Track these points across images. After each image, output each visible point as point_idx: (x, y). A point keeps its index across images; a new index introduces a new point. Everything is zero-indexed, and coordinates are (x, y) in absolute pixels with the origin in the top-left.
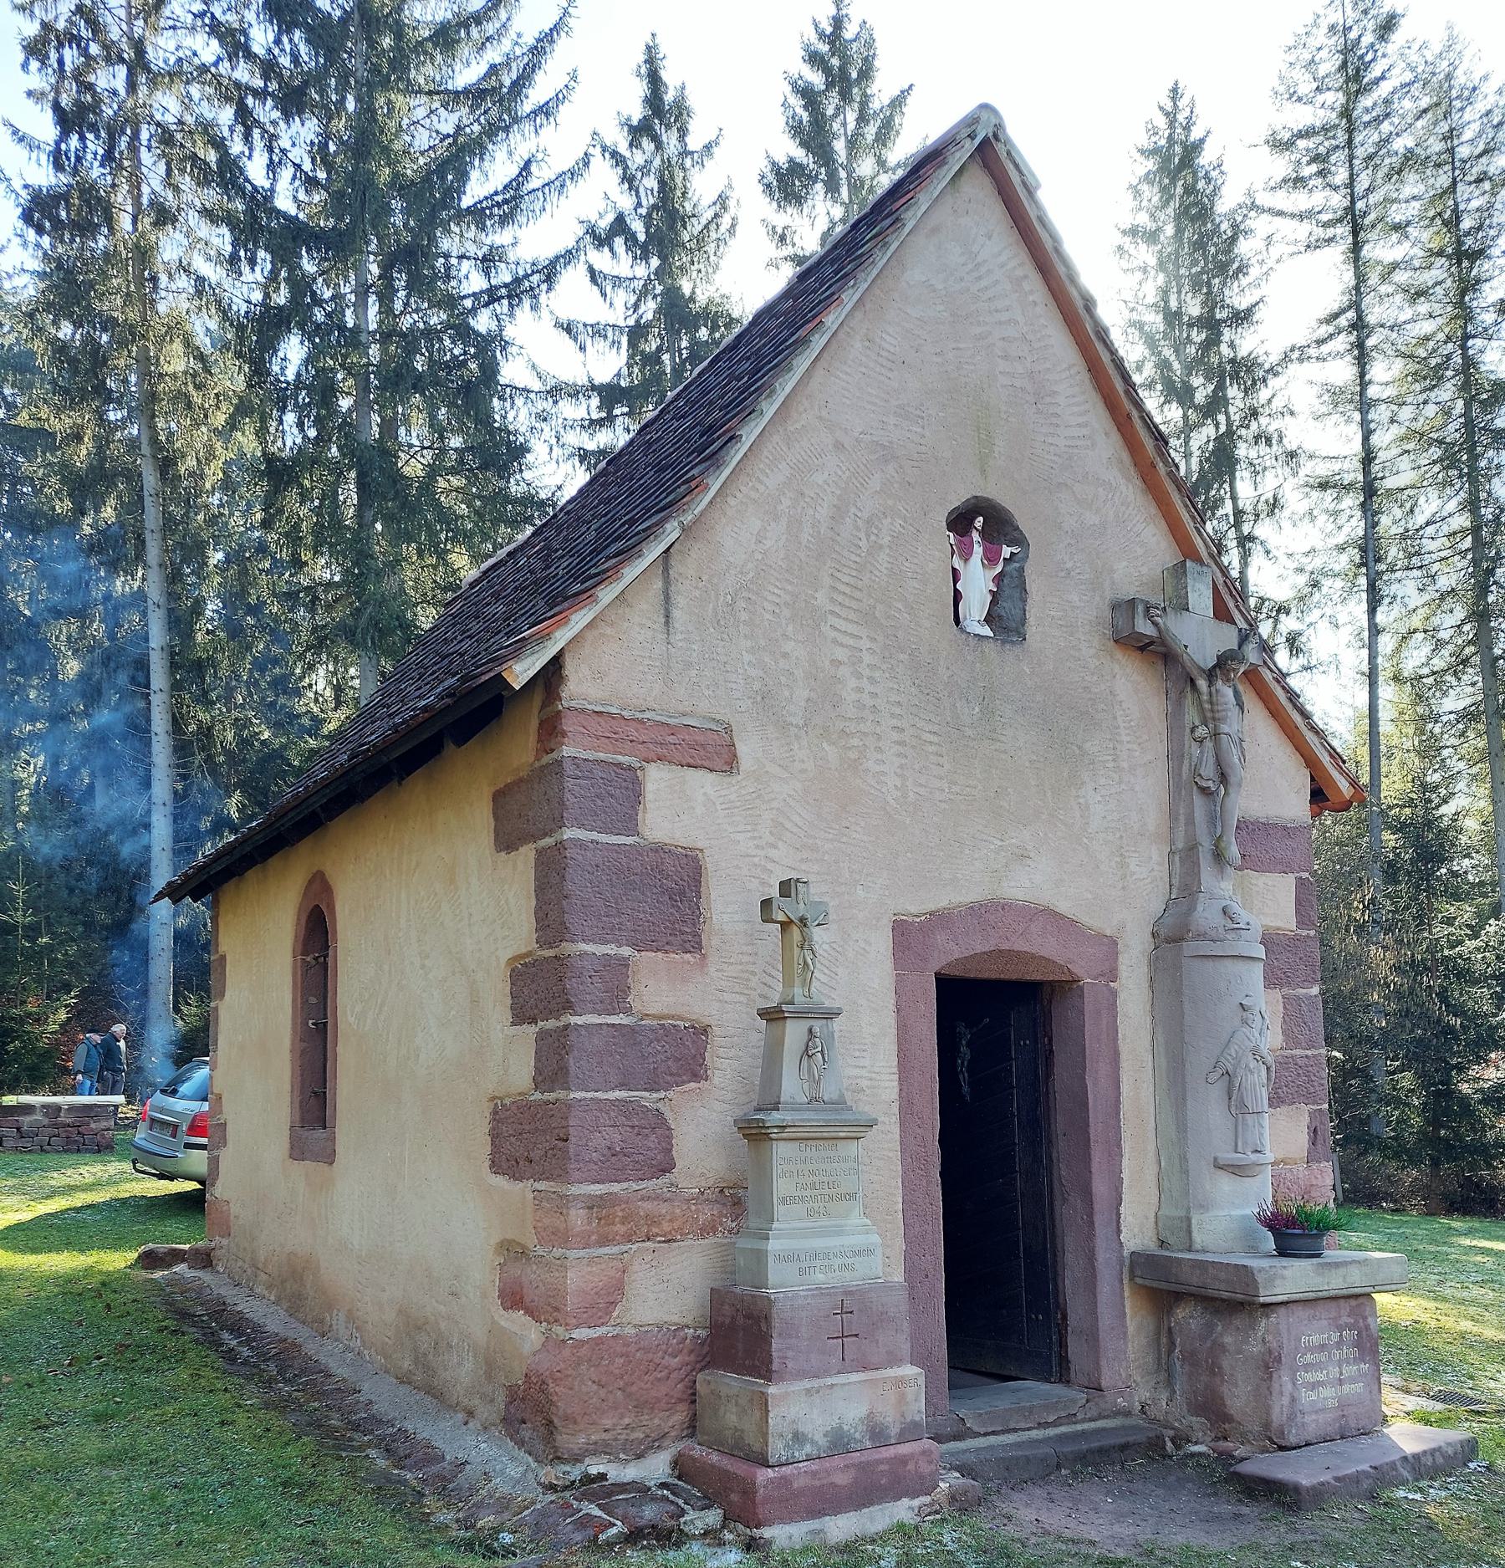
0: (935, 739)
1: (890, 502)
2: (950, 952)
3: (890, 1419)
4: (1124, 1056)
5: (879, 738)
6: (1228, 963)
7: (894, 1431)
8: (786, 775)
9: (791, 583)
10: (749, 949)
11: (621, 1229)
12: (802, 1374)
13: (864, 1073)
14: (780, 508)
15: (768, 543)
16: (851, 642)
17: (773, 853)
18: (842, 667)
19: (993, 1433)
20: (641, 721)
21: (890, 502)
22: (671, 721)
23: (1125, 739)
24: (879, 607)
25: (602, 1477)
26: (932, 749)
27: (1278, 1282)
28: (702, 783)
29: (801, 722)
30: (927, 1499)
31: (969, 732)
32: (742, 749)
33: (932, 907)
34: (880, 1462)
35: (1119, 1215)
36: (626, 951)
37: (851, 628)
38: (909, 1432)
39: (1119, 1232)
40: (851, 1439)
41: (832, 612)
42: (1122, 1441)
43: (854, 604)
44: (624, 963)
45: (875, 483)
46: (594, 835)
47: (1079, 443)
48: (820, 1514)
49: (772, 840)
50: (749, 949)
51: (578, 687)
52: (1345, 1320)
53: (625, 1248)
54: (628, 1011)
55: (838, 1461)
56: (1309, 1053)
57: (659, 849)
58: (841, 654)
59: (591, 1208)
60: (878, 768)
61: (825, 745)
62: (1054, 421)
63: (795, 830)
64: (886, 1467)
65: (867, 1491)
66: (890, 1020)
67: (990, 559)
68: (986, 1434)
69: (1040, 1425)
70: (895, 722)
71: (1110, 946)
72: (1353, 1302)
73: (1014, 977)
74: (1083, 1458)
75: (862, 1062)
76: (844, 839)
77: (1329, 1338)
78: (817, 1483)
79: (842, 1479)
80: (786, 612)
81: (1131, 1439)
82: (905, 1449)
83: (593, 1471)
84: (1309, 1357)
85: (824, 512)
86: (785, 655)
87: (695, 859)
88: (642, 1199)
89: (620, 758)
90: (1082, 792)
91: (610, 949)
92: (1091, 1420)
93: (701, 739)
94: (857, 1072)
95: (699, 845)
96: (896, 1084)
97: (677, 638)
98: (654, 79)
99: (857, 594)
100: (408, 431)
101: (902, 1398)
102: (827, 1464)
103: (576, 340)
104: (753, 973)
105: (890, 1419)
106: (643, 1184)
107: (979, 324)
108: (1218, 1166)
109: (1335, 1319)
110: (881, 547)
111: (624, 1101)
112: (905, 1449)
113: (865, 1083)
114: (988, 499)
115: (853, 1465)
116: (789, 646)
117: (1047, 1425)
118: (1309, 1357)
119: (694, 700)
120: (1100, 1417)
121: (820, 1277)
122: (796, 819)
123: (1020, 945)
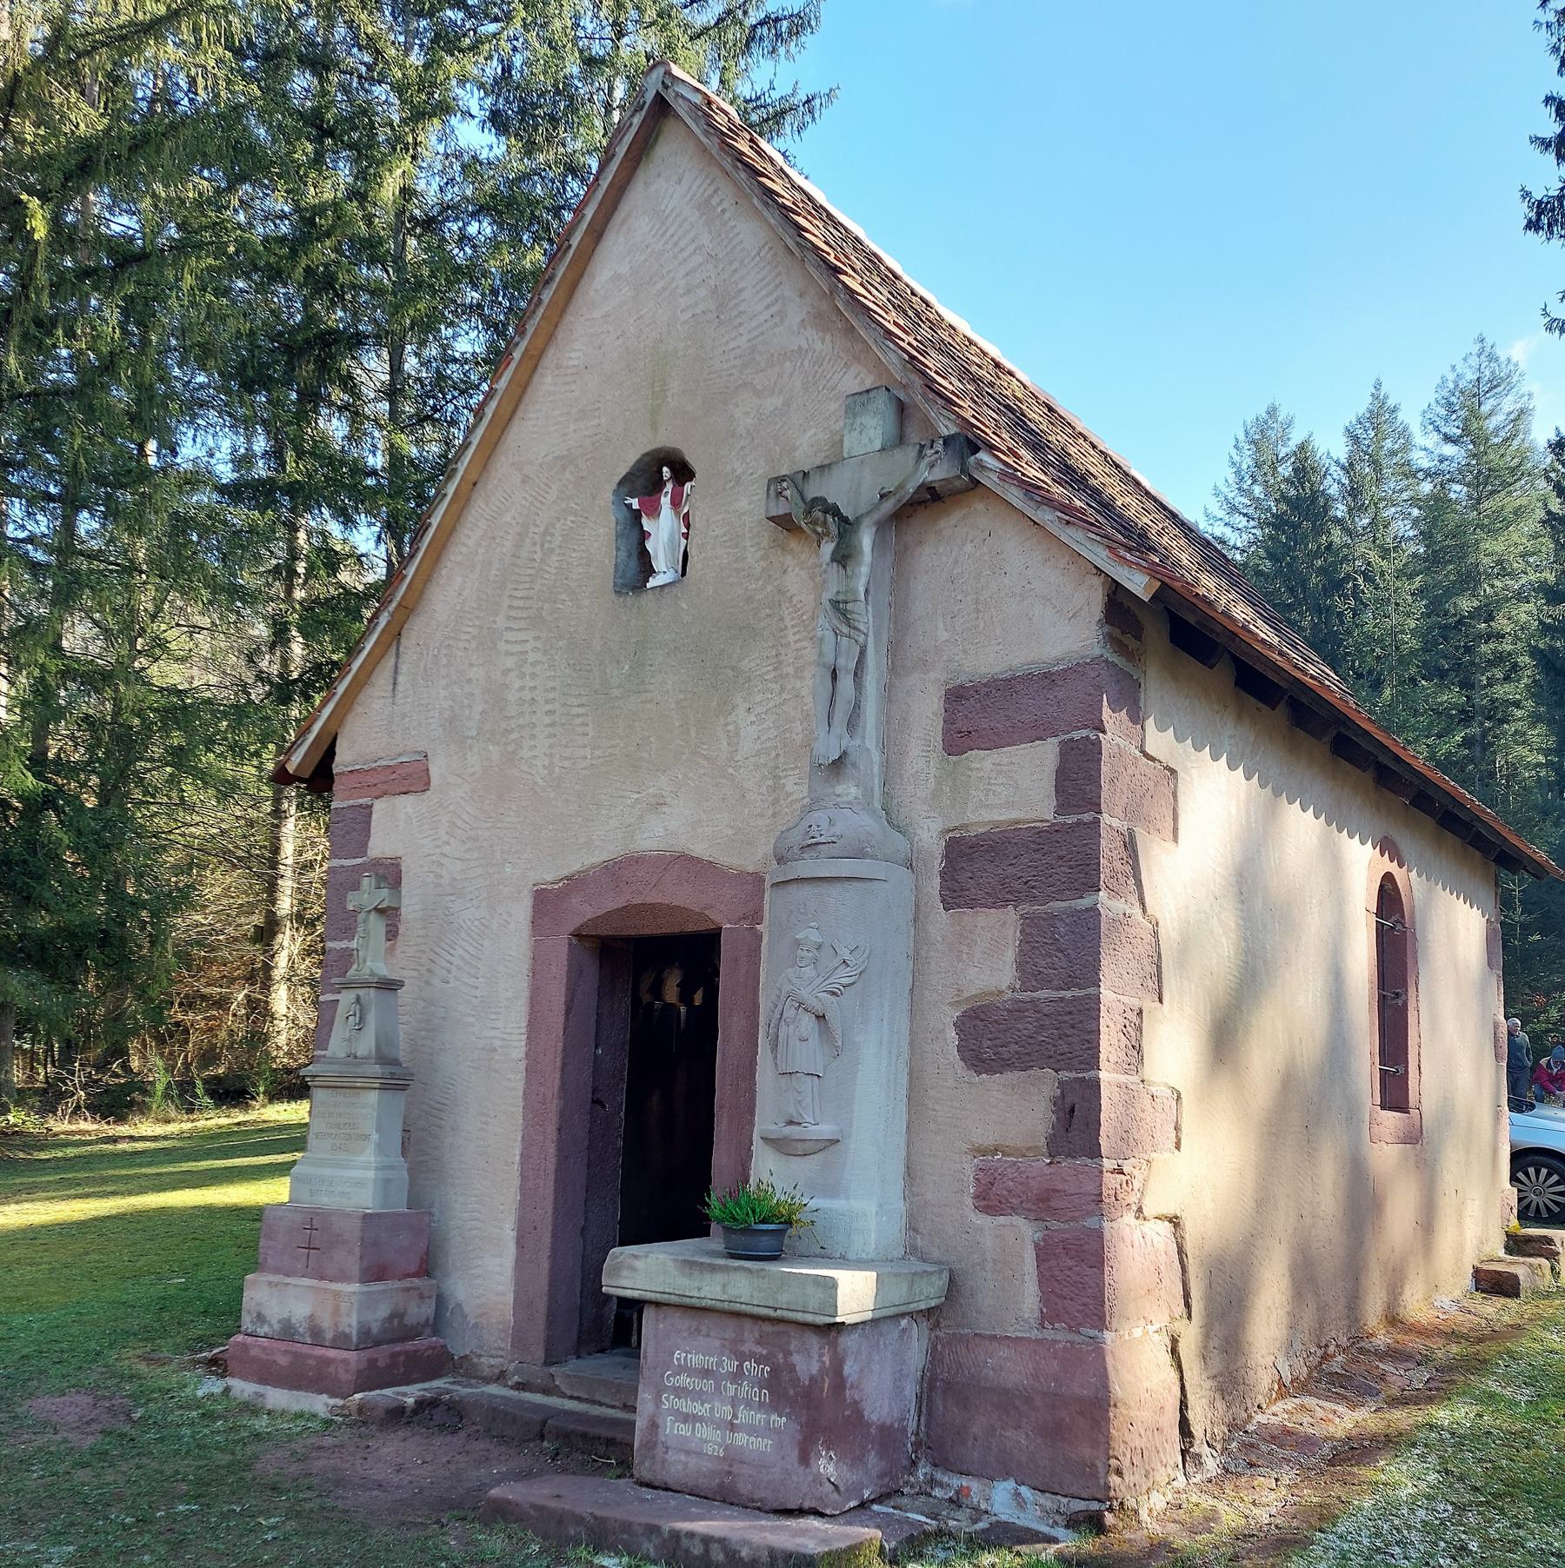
0: (581, 710)
2: (584, 911)
7: (329, 1335)
9: (477, 618)
12: (277, 1271)
13: (497, 1033)
17: (446, 849)
19: (579, 1399)
26: (578, 721)
27: (624, 1273)
28: (406, 804)
30: (340, 1402)
31: (616, 692)
33: (566, 872)
34: (310, 1356)
37: (521, 636)
38: (341, 1342)
40: (296, 1332)
42: (610, 1434)
43: (520, 614)
51: (344, 759)
52: (749, 1346)
55: (283, 1346)
56: (1068, 994)
58: (510, 662)
60: (530, 754)
65: (299, 1378)
66: (523, 985)
68: (571, 1398)
72: (768, 1328)
73: (676, 930)
74: (566, 1437)
77: (720, 1364)
79: (283, 1361)
80: (474, 644)
84: (684, 1380)
86: (469, 681)
90: (732, 718)
94: (493, 1033)
102: (275, 1344)
112: (332, 1353)
114: (647, 454)
118: (684, 1380)
122: (465, 817)
123: (653, 897)
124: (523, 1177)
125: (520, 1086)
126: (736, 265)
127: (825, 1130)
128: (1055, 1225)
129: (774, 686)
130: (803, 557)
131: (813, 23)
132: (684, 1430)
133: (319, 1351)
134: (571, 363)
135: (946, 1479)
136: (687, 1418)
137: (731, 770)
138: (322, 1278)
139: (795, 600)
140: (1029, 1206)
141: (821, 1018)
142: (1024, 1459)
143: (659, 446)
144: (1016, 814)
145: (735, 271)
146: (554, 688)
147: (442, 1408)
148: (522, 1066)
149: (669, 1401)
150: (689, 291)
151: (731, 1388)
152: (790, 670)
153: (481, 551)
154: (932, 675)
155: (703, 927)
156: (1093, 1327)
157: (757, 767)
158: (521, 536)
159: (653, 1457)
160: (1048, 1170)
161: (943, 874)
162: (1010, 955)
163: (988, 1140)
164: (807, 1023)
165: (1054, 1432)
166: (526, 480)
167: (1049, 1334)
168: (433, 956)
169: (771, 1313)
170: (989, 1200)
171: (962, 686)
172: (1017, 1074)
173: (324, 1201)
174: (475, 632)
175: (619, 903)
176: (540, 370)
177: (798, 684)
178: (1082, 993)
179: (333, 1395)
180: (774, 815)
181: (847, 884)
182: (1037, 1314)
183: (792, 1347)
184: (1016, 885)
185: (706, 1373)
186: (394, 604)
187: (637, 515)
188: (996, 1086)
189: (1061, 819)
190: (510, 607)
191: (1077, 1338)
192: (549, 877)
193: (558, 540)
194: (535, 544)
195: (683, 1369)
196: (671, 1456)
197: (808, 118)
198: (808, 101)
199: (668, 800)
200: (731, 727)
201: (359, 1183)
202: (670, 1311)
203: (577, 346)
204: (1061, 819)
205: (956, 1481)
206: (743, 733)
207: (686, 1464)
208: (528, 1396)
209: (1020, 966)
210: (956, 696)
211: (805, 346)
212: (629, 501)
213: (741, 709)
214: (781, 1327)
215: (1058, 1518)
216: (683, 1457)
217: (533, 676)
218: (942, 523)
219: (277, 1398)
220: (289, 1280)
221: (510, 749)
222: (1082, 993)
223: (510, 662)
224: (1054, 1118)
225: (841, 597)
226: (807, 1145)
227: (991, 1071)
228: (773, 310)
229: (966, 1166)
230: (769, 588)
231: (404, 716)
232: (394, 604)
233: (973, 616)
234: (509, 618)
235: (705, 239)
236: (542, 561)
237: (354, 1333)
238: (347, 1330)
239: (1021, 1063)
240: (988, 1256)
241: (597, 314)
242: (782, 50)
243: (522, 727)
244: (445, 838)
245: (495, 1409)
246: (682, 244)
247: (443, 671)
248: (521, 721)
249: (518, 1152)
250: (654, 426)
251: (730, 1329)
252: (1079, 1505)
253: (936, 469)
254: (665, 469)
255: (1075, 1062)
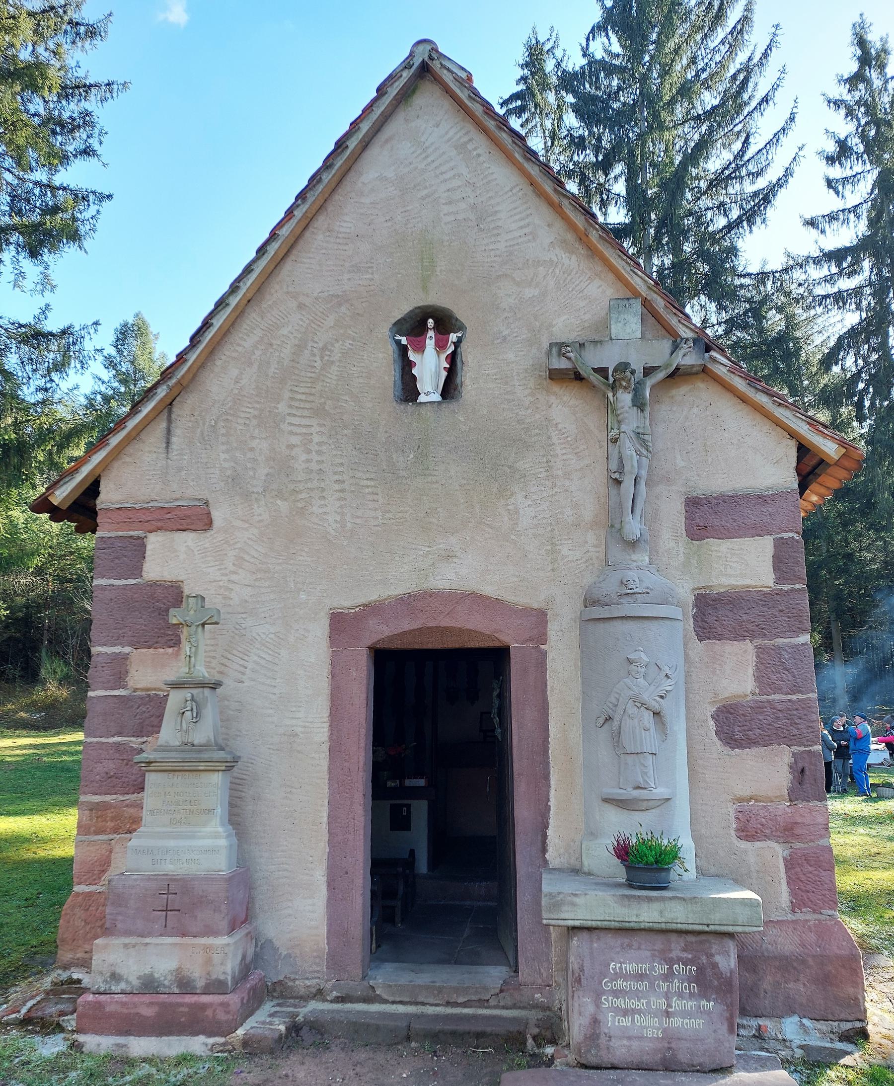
0: (369, 483)
1: (341, 331)
2: (381, 631)
3: (197, 975)
4: (551, 705)
5: (323, 490)
6: (617, 624)
7: (200, 984)
8: (247, 525)
9: (258, 403)
10: (212, 642)
11: (110, 824)
12: (128, 933)
14: (253, 357)
15: (243, 382)
16: (304, 430)
17: (234, 577)
18: (295, 449)
19: (401, 1002)
20: (147, 509)
21: (341, 331)
22: (166, 505)
23: (559, 452)
24: (329, 402)
25: (79, 981)
28: (186, 540)
29: (261, 490)
30: (221, 1040)
31: (402, 473)
32: (216, 515)
33: (364, 601)
35: (545, 837)
36: (127, 649)
39: (544, 850)
41: (289, 414)
42: (479, 1029)
43: (307, 406)
44: (125, 657)
45: (330, 321)
46: (112, 581)
47: (520, 240)
48: (127, 1033)
49: (232, 568)
50: (212, 642)
51: (108, 497)
53: (111, 837)
54: (124, 687)
55: (146, 999)
56: (794, 697)
57: (154, 584)
58: (294, 440)
59: (91, 810)
60: (321, 511)
61: (279, 502)
62: (495, 232)
63: (252, 560)
64: (186, 1010)
66: (324, 685)
67: (440, 346)
68: (393, 1003)
69: (448, 1004)
70: (337, 477)
71: (540, 617)
75: (298, 715)
76: (292, 562)
77: (652, 969)
78: (125, 1011)
79: (148, 1012)
80: (254, 422)
81: (488, 1029)
82: (205, 999)
83: (75, 976)
84: (620, 984)
85: (287, 351)
86: (252, 449)
87: (179, 587)
88: (127, 806)
89: (132, 533)
90: (512, 500)
91: (117, 649)
92: (504, 1008)
93: (188, 512)
94: (294, 722)
95: (180, 579)
96: (326, 730)
97: (173, 455)
98: (862, 43)
99: (311, 398)
100: (869, 304)
101: (209, 961)
102: (136, 999)
103: (818, 228)
104: (214, 658)
105: (197, 975)
106: (127, 797)
107: (426, 188)
108: (606, 800)
109: (662, 952)
110: (333, 362)
111: (118, 744)
112: (205, 999)
113: (299, 730)
114: (416, 308)
115: (157, 1003)
116: (254, 443)
117: (456, 1004)
118: (620, 984)
119: (182, 490)
120: (514, 1007)
121: (171, 867)
123: (445, 622)
124: (330, 833)
125: (325, 764)
126: (491, 194)
127: (661, 791)
128: (799, 845)
129: (547, 482)
130: (565, 399)
131: (103, 34)
132: (625, 1022)
133: (189, 999)
134: (342, 230)
135: (745, 1022)
136: (625, 1013)
137: (513, 537)
138: (184, 935)
139: (560, 426)
140: (779, 834)
141: (656, 714)
142: (804, 1002)
143: (431, 304)
144: (748, 582)
145: (491, 198)
146: (342, 464)
147: (305, 1030)
148: (326, 747)
149: (607, 1002)
150: (450, 203)
151: (664, 986)
152: (560, 473)
153: (258, 353)
154: (674, 488)
155: (497, 644)
156: (830, 909)
157: (535, 536)
158: (300, 348)
159: (598, 1045)
160: (789, 810)
161: (695, 617)
162: (750, 671)
163: (746, 792)
164: (648, 717)
165: (825, 981)
166: (301, 306)
167: (799, 916)
168: (225, 661)
169: (706, 928)
170: (748, 831)
171: (697, 497)
172: (763, 749)
173: (170, 868)
174: (256, 413)
175: (416, 625)
176: (311, 229)
177: (567, 483)
178: (804, 697)
179: (210, 1034)
180: (553, 570)
181: (661, 622)
182: (789, 904)
183: (713, 951)
184: (750, 626)
185: (640, 977)
186: (174, 381)
187: (403, 350)
188: (750, 757)
189: (779, 587)
190: (292, 399)
191: (820, 916)
192: (347, 604)
193: (337, 356)
194: (314, 355)
195: (618, 976)
196: (615, 1043)
197: (108, 95)
198: (108, 84)
199: (458, 554)
200: (510, 507)
201: (213, 850)
202: (602, 934)
203: (347, 218)
204: (779, 587)
205: (754, 1023)
206: (521, 512)
207: (630, 1046)
208: (349, 1006)
209: (757, 679)
210: (693, 503)
211: (555, 259)
212: (398, 337)
213: (520, 497)
214: (703, 937)
215: (832, 1036)
216: (625, 1042)
217: (319, 453)
218: (674, 392)
219: (140, 1046)
220: (147, 940)
221: (300, 505)
222: (804, 697)
223: (294, 440)
224: (791, 777)
225: (640, 431)
226: (650, 804)
227: (741, 746)
228: (526, 230)
229: (730, 810)
230: (537, 416)
231: (180, 469)
232: (174, 381)
233: (704, 453)
234: (290, 407)
235: (464, 170)
236: (322, 369)
237: (229, 978)
238: (222, 977)
239: (764, 741)
240: (753, 869)
241: (366, 200)
242: (79, 44)
243: (312, 489)
244: (232, 568)
245: (355, 1023)
246: (443, 169)
247: (222, 439)
248: (309, 485)
249: (325, 815)
250: (425, 288)
251: (659, 943)
252: (849, 1026)
253: (686, 358)
254: (431, 321)
255: (804, 740)
